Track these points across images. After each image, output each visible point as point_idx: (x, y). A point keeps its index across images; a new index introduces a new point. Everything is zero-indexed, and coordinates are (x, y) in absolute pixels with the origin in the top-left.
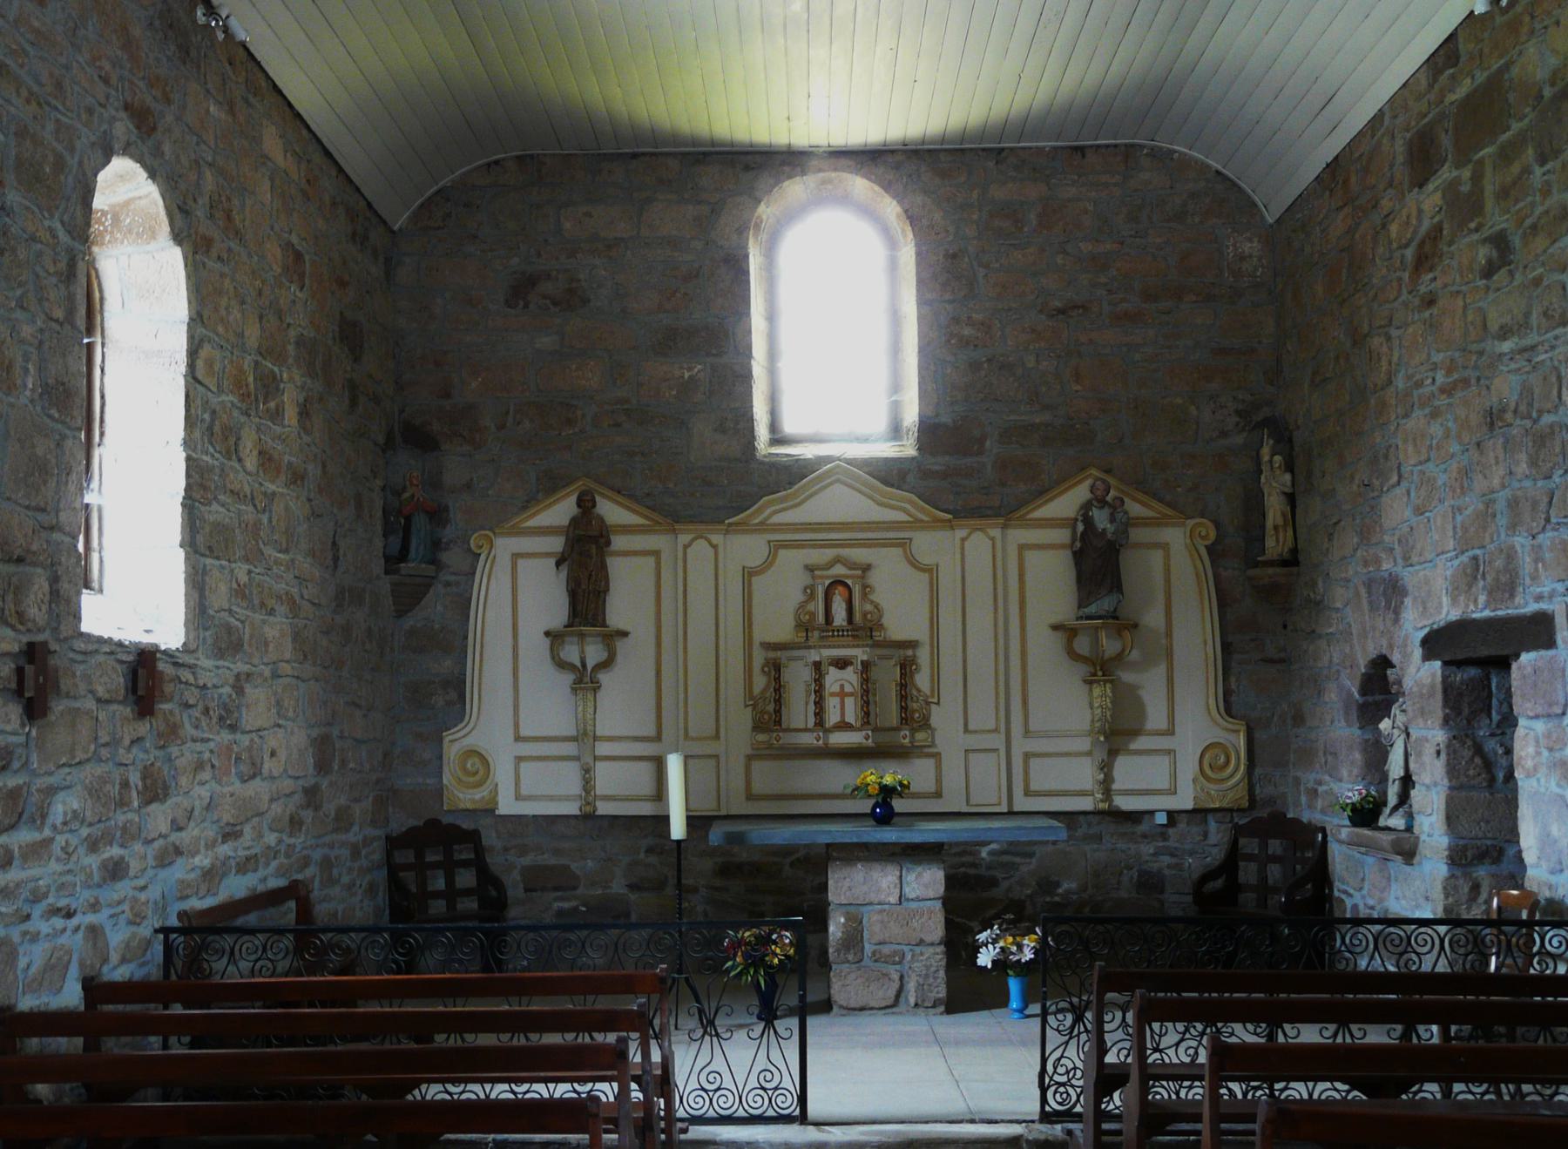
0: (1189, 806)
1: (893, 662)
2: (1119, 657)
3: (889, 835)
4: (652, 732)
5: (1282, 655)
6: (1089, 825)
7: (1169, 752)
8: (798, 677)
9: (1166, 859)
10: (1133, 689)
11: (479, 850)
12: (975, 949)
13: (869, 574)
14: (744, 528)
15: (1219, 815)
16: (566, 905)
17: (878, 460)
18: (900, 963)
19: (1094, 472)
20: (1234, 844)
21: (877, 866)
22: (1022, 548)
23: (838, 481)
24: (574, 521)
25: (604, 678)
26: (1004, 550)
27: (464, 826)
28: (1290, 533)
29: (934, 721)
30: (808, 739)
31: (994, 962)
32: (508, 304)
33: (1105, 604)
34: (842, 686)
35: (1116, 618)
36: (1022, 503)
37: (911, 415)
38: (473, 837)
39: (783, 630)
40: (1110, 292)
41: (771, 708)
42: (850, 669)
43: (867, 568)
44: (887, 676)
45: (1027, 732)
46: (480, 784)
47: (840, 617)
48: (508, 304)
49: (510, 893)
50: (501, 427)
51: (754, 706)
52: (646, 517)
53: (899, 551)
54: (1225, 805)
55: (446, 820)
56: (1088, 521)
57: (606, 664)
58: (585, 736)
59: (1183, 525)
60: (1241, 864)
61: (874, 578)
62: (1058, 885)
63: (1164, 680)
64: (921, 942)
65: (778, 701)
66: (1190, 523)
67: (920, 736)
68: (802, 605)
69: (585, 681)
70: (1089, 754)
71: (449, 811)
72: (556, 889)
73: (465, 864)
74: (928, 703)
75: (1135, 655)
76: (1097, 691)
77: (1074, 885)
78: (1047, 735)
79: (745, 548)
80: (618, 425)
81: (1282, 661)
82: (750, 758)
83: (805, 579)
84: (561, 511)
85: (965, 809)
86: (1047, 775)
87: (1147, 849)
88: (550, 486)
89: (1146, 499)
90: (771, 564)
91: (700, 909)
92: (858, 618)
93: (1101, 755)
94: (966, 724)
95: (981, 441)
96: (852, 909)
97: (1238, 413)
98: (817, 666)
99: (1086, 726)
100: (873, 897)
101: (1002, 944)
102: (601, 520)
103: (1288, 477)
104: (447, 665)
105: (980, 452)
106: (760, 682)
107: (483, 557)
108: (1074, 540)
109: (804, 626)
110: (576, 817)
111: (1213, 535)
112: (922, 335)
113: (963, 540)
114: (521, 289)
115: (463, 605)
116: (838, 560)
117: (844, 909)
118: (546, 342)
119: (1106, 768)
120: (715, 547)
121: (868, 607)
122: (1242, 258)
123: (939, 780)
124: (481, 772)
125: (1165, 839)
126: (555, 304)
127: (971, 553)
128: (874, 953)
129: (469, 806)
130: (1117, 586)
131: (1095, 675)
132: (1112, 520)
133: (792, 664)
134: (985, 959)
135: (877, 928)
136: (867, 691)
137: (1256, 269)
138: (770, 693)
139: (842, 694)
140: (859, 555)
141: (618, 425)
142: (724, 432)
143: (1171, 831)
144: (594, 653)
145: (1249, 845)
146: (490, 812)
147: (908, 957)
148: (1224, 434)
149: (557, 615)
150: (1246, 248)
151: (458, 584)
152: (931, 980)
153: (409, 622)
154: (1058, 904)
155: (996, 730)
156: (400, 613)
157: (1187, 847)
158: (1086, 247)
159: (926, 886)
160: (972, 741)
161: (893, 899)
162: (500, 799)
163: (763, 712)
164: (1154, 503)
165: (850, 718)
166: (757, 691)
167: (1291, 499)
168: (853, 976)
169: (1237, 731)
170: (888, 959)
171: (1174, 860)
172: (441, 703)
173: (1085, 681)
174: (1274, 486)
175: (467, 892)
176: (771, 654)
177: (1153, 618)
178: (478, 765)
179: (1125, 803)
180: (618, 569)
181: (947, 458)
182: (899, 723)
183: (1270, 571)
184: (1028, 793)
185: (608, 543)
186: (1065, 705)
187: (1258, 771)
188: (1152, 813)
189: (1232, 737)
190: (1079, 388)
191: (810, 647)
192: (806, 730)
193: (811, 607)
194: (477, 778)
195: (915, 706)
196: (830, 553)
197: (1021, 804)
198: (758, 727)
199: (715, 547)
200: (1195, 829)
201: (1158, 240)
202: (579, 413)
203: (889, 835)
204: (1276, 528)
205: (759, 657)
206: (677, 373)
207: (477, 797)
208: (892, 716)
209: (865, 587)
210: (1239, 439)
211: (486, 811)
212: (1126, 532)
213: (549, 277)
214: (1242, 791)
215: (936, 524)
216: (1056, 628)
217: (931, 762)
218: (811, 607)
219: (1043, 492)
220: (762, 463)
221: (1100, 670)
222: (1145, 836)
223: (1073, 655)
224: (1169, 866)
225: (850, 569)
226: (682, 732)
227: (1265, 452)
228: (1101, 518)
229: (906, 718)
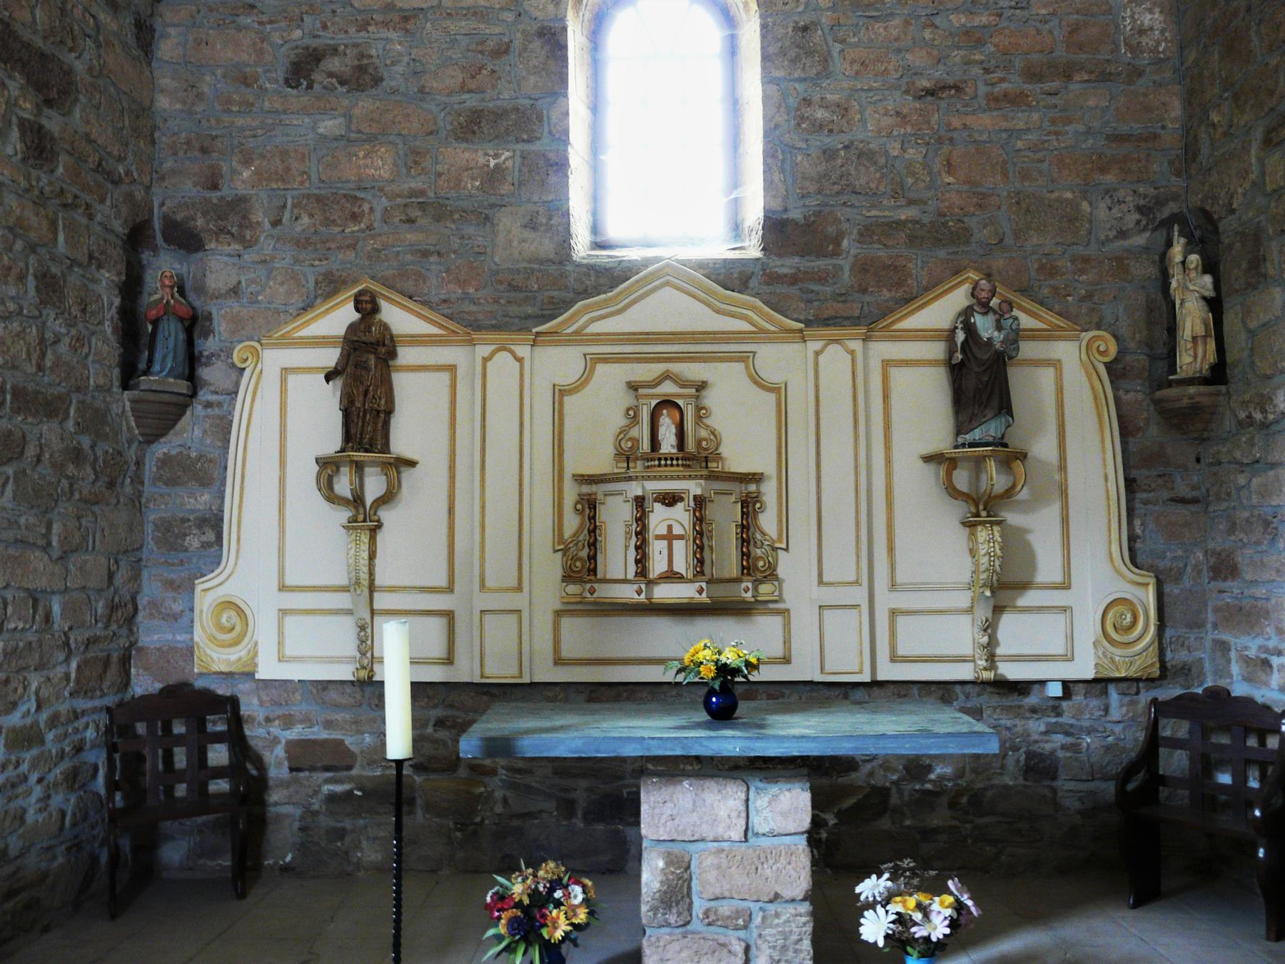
0: (1090, 674)
1: (733, 498)
2: (1009, 493)
3: (730, 742)
4: (442, 581)
5: (1195, 494)
6: (967, 696)
7: (1064, 609)
8: (616, 516)
9: (1059, 739)
10: (1022, 532)
11: (237, 721)
12: (858, 909)
13: (704, 393)
14: (555, 338)
15: (1124, 685)
16: (339, 788)
17: (715, 262)
18: (745, 927)
19: (974, 276)
20: (1154, 728)
21: (711, 785)
22: (887, 364)
23: (667, 284)
24: (352, 328)
25: (385, 515)
26: (866, 366)
27: (220, 692)
28: (1212, 345)
29: (780, 572)
30: (628, 593)
31: (887, 937)
32: (287, 82)
33: (991, 429)
34: (670, 527)
35: (1006, 445)
36: (886, 312)
37: (754, 214)
38: (232, 704)
39: (602, 460)
40: (987, 71)
41: (584, 553)
42: (680, 506)
43: (701, 386)
44: (726, 515)
45: (893, 586)
46: (236, 642)
47: (668, 443)
48: (287, 82)
49: (273, 773)
50: (276, 223)
51: (565, 551)
52: (441, 326)
53: (739, 367)
54: (1132, 673)
55: (199, 684)
56: (970, 329)
57: (388, 498)
58: (367, 585)
59: (1077, 338)
60: (1162, 751)
61: (711, 399)
62: (929, 769)
63: (1058, 520)
64: (776, 897)
65: (593, 545)
66: (1087, 336)
67: (765, 588)
68: (624, 431)
69: (365, 519)
70: (970, 611)
71: (201, 674)
72: (327, 769)
73: (218, 738)
74: (775, 549)
75: (1024, 494)
76: (982, 534)
77: (948, 770)
78: (918, 588)
79: (559, 363)
80: (411, 221)
81: (1195, 501)
82: (559, 614)
83: (628, 400)
84: (338, 318)
85: (819, 678)
86: (914, 637)
87: (1036, 726)
88: (330, 286)
89: (1035, 307)
90: (587, 381)
91: (498, 794)
92: (691, 446)
93: (983, 613)
94: (820, 575)
95: (837, 241)
96: (676, 848)
97: (1139, 209)
98: (640, 502)
99: (966, 577)
100: (706, 831)
101: (895, 907)
102: (386, 327)
103: (1208, 279)
104: (204, 499)
105: (836, 254)
106: (572, 523)
107: (247, 373)
108: (951, 352)
109: (626, 456)
110: (352, 682)
111: (1113, 349)
112: (767, 119)
113: (817, 354)
114: (302, 69)
115: (223, 429)
116: (666, 376)
117: (663, 848)
118: (330, 125)
119: (990, 627)
120: (520, 360)
121: (703, 433)
122: (1142, 32)
123: (787, 642)
124: (238, 629)
125: (1059, 715)
126: (342, 83)
127: (825, 368)
128: (706, 914)
129: (224, 668)
130: (1005, 408)
131: (977, 515)
132: (999, 327)
133: (609, 500)
134: (874, 928)
135: (711, 876)
136: (701, 533)
137: (1158, 43)
138: (584, 535)
139: (670, 537)
140: (693, 371)
141: (411, 221)
142: (534, 229)
143: (1064, 704)
144: (374, 486)
145: (1169, 728)
146: (250, 675)
147: (757, 920)
148: (1122, 234)
149: (331, 441)
150: (1147, 19)
151: (220, 404)
152: (791, 954)
153: (161, 449)
154: (929, 791)
155: (857, 582)
156: (152, 437)
157: (1086, 724)
158: (959, 20)
159: (784, 815)
160: (829, 595)
161: (737, 834)
162: (261, 660)
163: (575, 558)
164: (1043, 312)
165: (680, 566)
166: (569, 531)
167: (1214, 305)
168: (676, 946)
169: (1148, 584)
170: (727, 923)
171: (1069, 740)
172: (196, 544)
173: (963, 524)
174: (1191, 295)
175: (219, 773)
176: (585, 489)
177: (1043, 448)
178: (235, 619)
179: (1012, 672)
180: (403, 384)
181: (797, 259)
182: (740, 580)
183: (1192, 390)
184: (894, 658)
185: (393, 354)
186: (940, 552)
187: (1169, 633)
188: (1043, 683)
189: (1139, 592)
190: (951, 179)
191: (630, 479)
192: (625, 581)
193: (634, 433)
194: (233, 634)
195: (759, 552)
196: (658, 369)
197: (887, 672)
198: (568, 577)
199: (520, 360)
200: (1094, 703)
201: (1044, 12)
202: (366, 207)
203: (730, 742)
204: (1194, 339)
205: (571, 493)
206: (482, 160)
207: (233, 658)
208: (728, 560)
209: (699, 408)
210: (1140, 240)
211: (243, 674)
212: (1016, 341)
213: (334, 51)
214: (1152, 658)
215: (786, 335)
216: (928, 459)
217: (777, 621)
218: (634, 433)
219: (910, 300)
220: (579, 265)
221: (982, 509)
222: (1034, 710)
223: (952, 491)
224: (1063, 747)
225: (683, 386)
226: (477, 580)
227: (1177, 251)
228: (985, 326)
229: (748, 568)
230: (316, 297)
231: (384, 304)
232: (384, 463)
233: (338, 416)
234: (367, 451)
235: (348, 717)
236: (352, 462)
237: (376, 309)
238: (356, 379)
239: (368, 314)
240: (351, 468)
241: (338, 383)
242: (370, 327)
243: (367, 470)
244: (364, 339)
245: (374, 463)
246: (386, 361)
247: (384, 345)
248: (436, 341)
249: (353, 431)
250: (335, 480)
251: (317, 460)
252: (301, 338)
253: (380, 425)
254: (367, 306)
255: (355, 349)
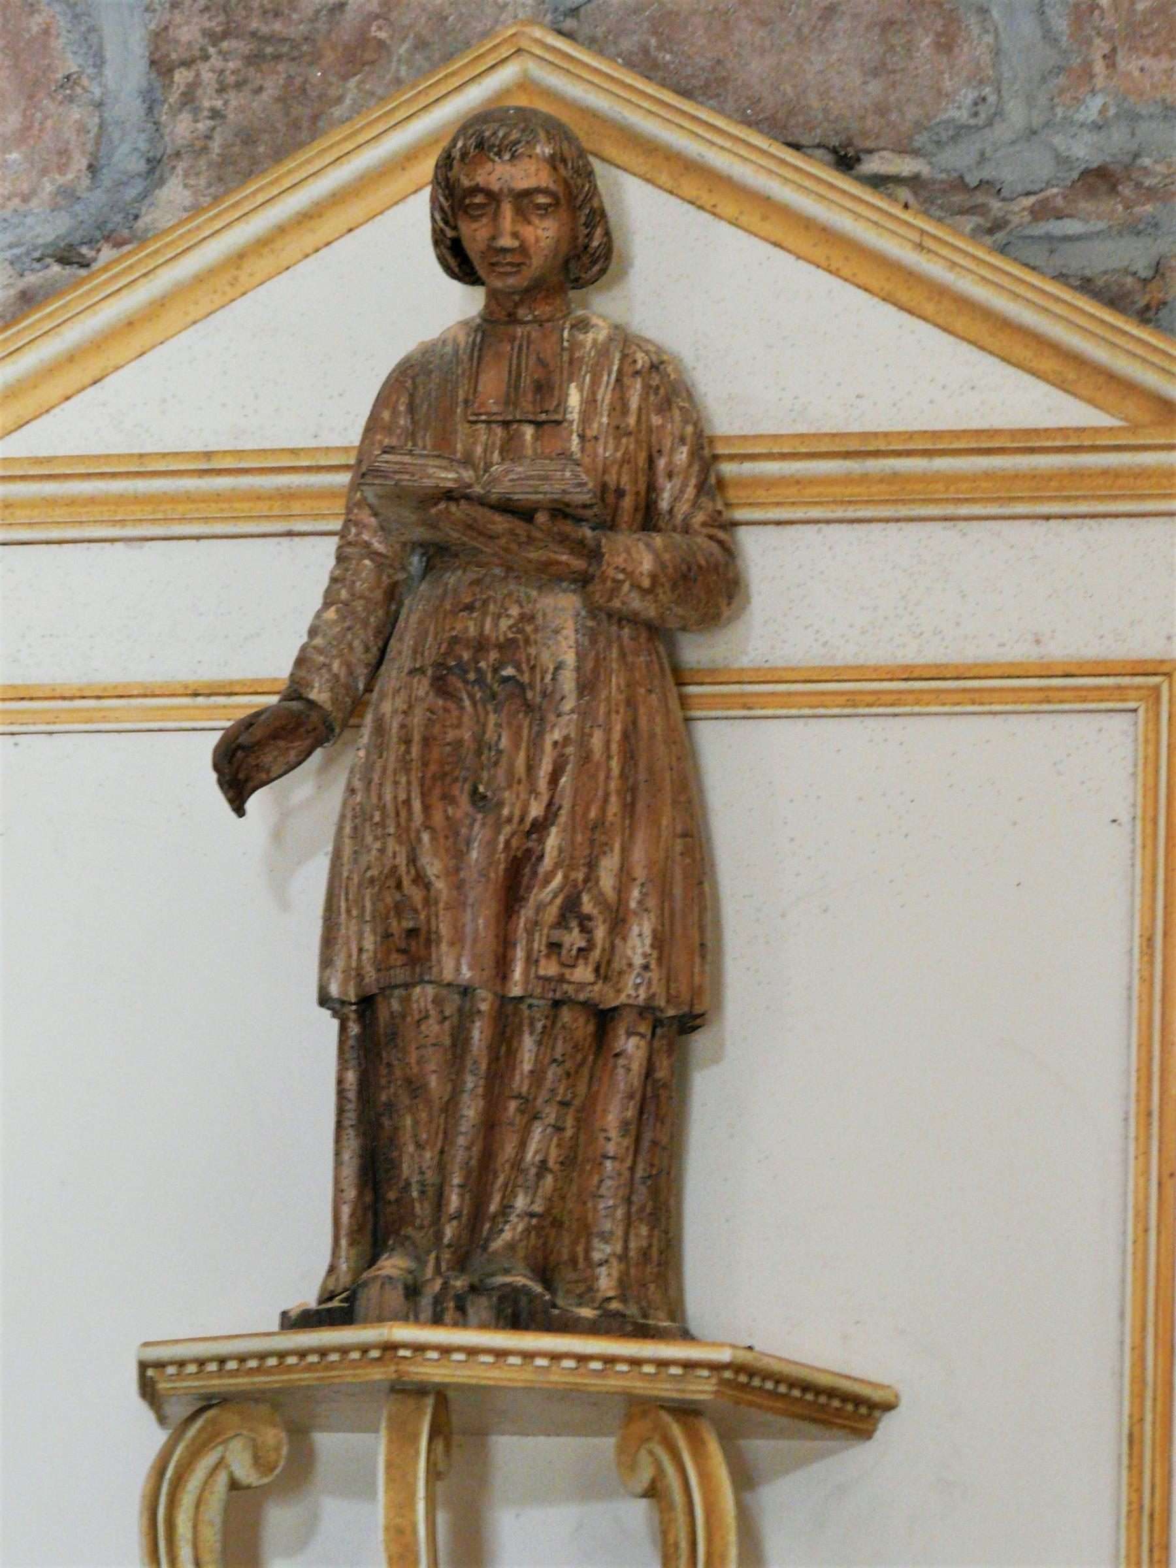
24: (418, 394)
88: (256, 87)
102: (662, 383)
149: (261, 1236)
180: (779, 799)
185: (711, 586)
230: (155, 168)
231: (641, 209)
232: (638, 1408)
233: (313, 1049)
234: (515, 1314)
235: (540, 1130)
236: (408, 1391)
237: (589, 255)
238: (447, 775)
239: (538, 290)
240: (402, 1437)
241: (309, 799)
242: (545, 389)
243: (513, 1453)
244: (512, 478)
245: (565, 1408)
246: (657, 633)
247: (649, 518)
248: (1040, 486)
249: (414, 1163)
250: (279, 1518)
251: (150, 1383)
252: (47, 469)
253: (614, 1115)
254: (526, 234)
255: (437, 555)
